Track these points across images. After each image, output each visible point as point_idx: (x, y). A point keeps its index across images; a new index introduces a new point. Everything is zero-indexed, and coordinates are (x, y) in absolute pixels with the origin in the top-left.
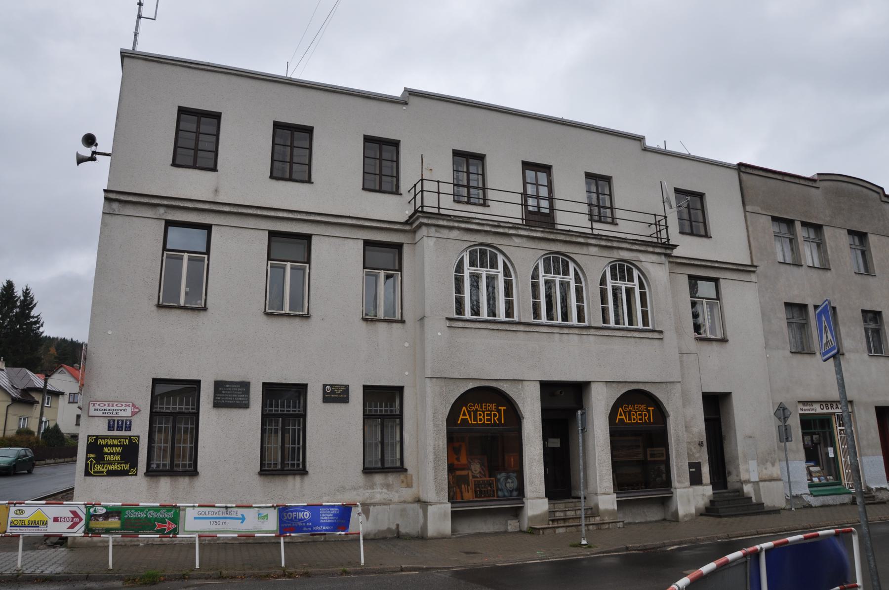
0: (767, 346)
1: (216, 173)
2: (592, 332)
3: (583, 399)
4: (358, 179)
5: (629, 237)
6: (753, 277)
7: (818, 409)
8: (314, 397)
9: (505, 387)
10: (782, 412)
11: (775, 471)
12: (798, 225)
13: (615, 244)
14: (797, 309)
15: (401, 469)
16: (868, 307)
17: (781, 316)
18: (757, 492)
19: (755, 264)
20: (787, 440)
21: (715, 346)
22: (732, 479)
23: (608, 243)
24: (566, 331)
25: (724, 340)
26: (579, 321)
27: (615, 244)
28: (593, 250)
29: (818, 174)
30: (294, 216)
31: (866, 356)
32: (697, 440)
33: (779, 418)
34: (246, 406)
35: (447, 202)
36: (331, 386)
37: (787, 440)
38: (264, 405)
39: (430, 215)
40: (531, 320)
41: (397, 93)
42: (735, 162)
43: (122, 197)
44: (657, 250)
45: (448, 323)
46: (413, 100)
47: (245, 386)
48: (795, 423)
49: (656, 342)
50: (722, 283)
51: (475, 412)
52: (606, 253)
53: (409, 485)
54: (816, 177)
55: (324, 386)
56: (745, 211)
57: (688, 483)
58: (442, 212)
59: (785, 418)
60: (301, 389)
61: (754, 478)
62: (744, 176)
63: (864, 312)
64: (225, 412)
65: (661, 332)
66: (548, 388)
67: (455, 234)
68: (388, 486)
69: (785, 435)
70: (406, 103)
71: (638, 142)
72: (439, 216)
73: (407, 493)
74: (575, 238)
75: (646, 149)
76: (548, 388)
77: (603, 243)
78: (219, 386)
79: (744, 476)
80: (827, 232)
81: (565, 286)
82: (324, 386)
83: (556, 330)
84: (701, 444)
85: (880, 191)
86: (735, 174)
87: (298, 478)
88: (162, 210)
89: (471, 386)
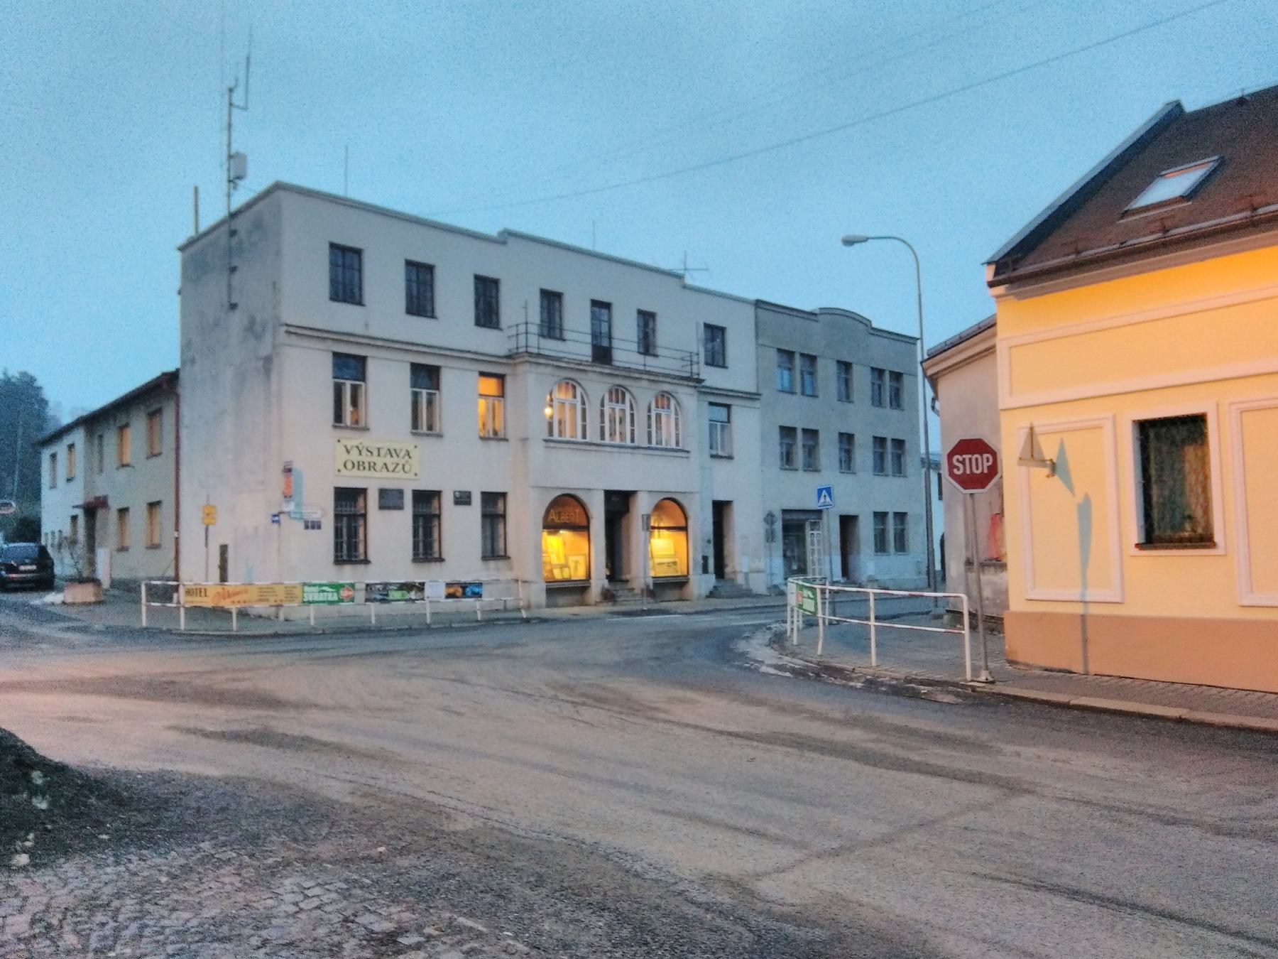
0: (763, 462)
1: (816, 474)
2: (641, 451)
3: (630, 505)
4: (472, 321)
5: (672, 373)
6: (757, 404)
7: (795, 516)
8: (447, 500)
9: (581, 495)
10: (770, 518)
11: (761, 564)
12: (797, 357)
13: (661, 379)
14: (787, 432)
15: (505, 557)
16: (843, 431)
17: (776, 435)
18: (747, 579)
19: (760, 392)
20: (772, 540)
21: (724, 462)
22: (728, 570)
23: (654, 377)
24: (622, 450)
25: (730, 458)
26: (560, 436)
27: (661, 379)
28: (644, 384)
29: (821, 309)
30: (430, 349)
31: (837, 473)
32: (706, 538)
33: (767, 523)
34: (400, 508)
35: (533, 340)
36: (460, 492)
37: (772, 540)
38: (414, 506)
39: (531, 354)
40: (598, 441)
41: (493, 231)
42: (753, 296)
43: (299, 331)
44: (691, 384)
45: (544, 443)
46: (511, 240)
47: (401, 492)
48: (778, 526)
49: (685, 459)
50: (734, 410)
51: (559, 513)
52: (654, 386)
53: (511, 569)
54: (817, 312)
55: (455, 492)
56: (757, 344)
57: (701, 572)
58: (542, 352)
59: (772, 523)
60: (437, 494)
61: (745, 570)
62: (760, 311)
63: (841, 434)
64: (386, 513)
65: (688, 452)
66: (609, 495)
67: (549, 370)
68: (498, 569)
69: (770, 536)
70: (504, 243)
71: (678, 280)
72: (539, 355)
73: (510, 575)
74: (629, 373)
75: (685, 287)
76: (609, 495)
77: (652, 378)
78: (383, 493)
79: (738, 569)
80: (820, 362)
81: (623, 411)
82: (455, 492)
83: (615, 450)
84: (709, 541)
85: (868, 323)
86: (750, 311)
87: (438, 564)
88: (329, 343)
89: (559, 493)
